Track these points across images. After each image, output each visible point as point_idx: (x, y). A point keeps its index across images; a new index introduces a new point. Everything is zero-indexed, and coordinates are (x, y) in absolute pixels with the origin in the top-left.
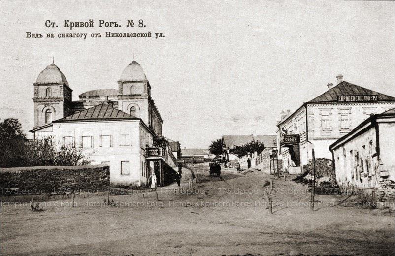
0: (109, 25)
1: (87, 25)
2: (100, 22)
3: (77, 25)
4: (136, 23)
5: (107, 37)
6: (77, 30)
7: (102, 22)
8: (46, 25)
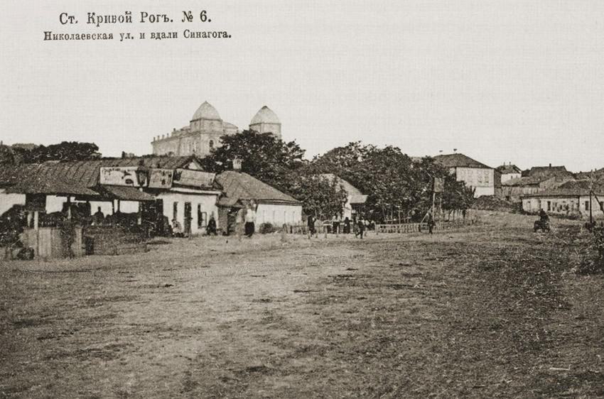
0: (154, 19)
5: (45, 39)
6: (105, 28)
7: (144, 15)
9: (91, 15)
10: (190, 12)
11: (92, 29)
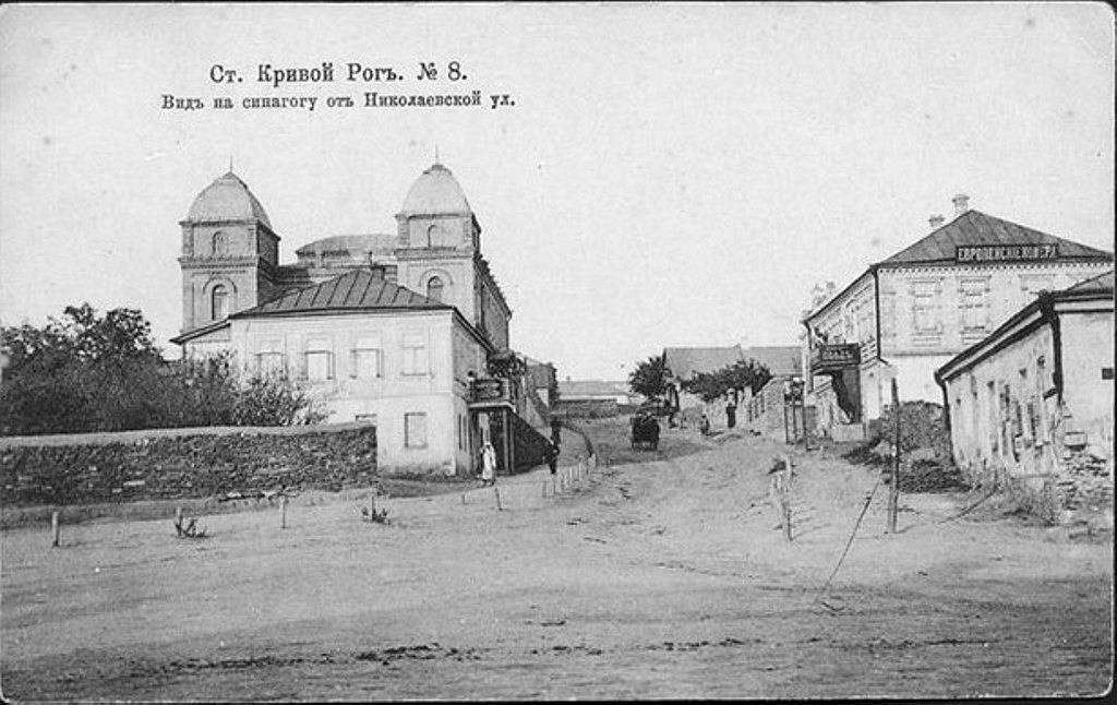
0: (372, 75)
3: (291, 75)
5: (165, 107)
6: (288, 89)
7: (355, 69)
9: (264, 69)
10: (432, 65)
11: (267, 90)
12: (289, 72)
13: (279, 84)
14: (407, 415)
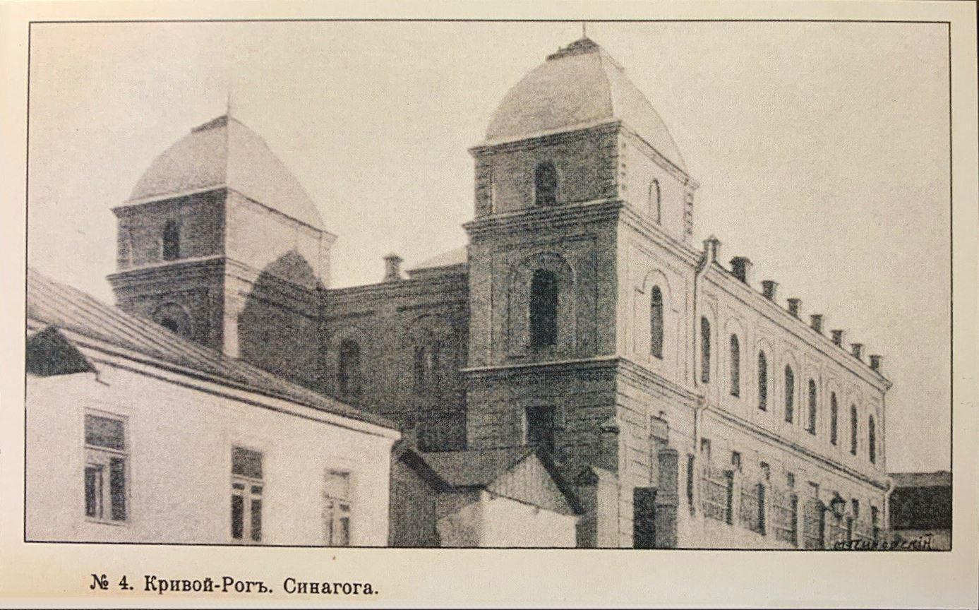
1: (197, 588)
2: (225, 582)
3: (175, 586)
4: (114, 581)
8: (345, 592)
9: (150, 580)
12: (172, 582)
13: (163, 592)
14: (949, 23)
